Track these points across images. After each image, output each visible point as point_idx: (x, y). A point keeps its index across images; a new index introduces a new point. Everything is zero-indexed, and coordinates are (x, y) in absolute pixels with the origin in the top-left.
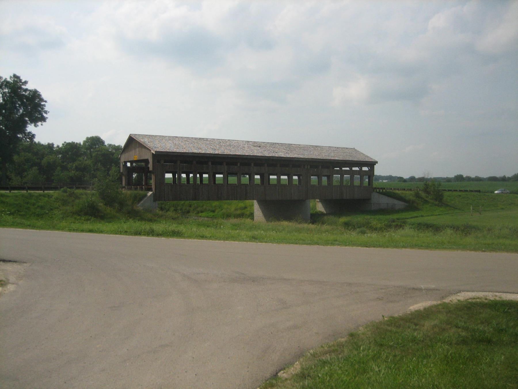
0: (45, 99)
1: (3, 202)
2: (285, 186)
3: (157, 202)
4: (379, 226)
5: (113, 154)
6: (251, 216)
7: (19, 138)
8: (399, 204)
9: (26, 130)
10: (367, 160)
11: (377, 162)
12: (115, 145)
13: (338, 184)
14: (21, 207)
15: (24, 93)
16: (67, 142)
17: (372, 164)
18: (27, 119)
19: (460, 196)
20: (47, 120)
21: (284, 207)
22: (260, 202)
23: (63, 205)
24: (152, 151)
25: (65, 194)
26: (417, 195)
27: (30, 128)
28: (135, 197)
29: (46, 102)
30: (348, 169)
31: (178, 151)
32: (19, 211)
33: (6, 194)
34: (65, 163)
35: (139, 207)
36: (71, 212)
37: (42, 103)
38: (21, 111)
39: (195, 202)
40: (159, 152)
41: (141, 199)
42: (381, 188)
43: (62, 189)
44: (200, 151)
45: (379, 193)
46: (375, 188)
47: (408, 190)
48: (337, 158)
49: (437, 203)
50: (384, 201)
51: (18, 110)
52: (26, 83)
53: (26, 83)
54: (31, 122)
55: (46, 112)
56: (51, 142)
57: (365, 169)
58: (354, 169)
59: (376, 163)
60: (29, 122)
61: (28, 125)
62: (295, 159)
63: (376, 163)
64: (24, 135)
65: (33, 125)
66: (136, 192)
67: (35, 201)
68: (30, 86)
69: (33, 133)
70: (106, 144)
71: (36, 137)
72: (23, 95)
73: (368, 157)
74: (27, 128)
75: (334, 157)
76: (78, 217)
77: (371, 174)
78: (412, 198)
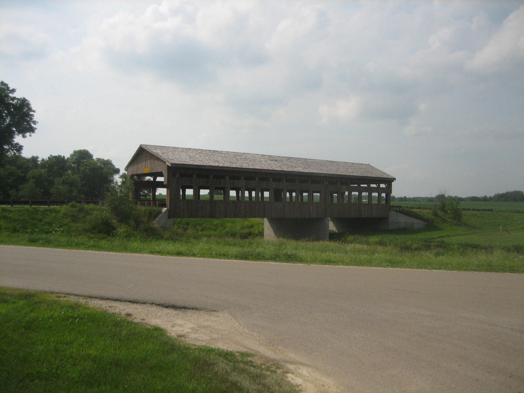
0: (33, 109)
1: (5, 218)
2: (189, 201)
3: (172, 219)
4: (415, 245)
5: (101, 168)
6: (261, 234)
7: (6, 149)
8: (418, 224)
9: (13, 141)
10: (385, 176)
11: (395, 179)
12: (103, 160)
13: (376, 202)
14: (26, 223)
15: (11, 101)
16: (54, 155)
17: (389, 181)
18: (14, 129)
19: (475, 215)
20: (36, 131)
21: (299, 226)
22: (272, 221)
23: (73, 221)
24: (167, 164)
25: (74, 209)
26: (435, 214)
27: (18, 139)
28: (151, 213)
29: (34, 111)
30: (366, 186)
31: (195, 164)
32: (25, 228)
33: (8, 209)
34: (51, 178)
35: (156, 224)
36: (83, 230)
37: (31, 113)
38: (8, 121)
39: (192, 219)
40: (175, 164)
41: (156, 216)
42: (398, 207)
43: (70, 204)
44: (216, 164)
45: (396, 211)
46: (392, 206)
47: (423, 208)
48: (355, 174)
49: (456, 222)
50: (403, 219)
51: (5, 120)
52: (13, 91)
53: (13, 91)
54: (19, 133)
55: (35, 123)
56: (35, 156)
57: (383, 186)
58: (372, 186)
59: (393, 179)
60: (16, 133)
61: (16, 136)
62: (315, 175)
63: (393, 179)
64: (10, 146)
65: (21, 135)
66: (150, 208)
67: (41, 217)
68: (18, 95)
69: (21, 144)
70: (95, 157)
71: (24, 148)
72: (11, 104)
73: (385, 173)
74: (14, 140)
75: (352, 172)
76: (92, 236)
77: (388, 190)
78: (430, 217)
